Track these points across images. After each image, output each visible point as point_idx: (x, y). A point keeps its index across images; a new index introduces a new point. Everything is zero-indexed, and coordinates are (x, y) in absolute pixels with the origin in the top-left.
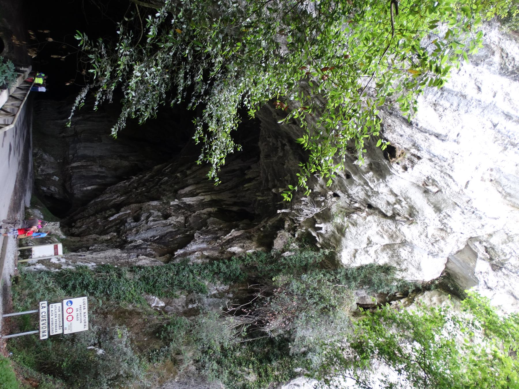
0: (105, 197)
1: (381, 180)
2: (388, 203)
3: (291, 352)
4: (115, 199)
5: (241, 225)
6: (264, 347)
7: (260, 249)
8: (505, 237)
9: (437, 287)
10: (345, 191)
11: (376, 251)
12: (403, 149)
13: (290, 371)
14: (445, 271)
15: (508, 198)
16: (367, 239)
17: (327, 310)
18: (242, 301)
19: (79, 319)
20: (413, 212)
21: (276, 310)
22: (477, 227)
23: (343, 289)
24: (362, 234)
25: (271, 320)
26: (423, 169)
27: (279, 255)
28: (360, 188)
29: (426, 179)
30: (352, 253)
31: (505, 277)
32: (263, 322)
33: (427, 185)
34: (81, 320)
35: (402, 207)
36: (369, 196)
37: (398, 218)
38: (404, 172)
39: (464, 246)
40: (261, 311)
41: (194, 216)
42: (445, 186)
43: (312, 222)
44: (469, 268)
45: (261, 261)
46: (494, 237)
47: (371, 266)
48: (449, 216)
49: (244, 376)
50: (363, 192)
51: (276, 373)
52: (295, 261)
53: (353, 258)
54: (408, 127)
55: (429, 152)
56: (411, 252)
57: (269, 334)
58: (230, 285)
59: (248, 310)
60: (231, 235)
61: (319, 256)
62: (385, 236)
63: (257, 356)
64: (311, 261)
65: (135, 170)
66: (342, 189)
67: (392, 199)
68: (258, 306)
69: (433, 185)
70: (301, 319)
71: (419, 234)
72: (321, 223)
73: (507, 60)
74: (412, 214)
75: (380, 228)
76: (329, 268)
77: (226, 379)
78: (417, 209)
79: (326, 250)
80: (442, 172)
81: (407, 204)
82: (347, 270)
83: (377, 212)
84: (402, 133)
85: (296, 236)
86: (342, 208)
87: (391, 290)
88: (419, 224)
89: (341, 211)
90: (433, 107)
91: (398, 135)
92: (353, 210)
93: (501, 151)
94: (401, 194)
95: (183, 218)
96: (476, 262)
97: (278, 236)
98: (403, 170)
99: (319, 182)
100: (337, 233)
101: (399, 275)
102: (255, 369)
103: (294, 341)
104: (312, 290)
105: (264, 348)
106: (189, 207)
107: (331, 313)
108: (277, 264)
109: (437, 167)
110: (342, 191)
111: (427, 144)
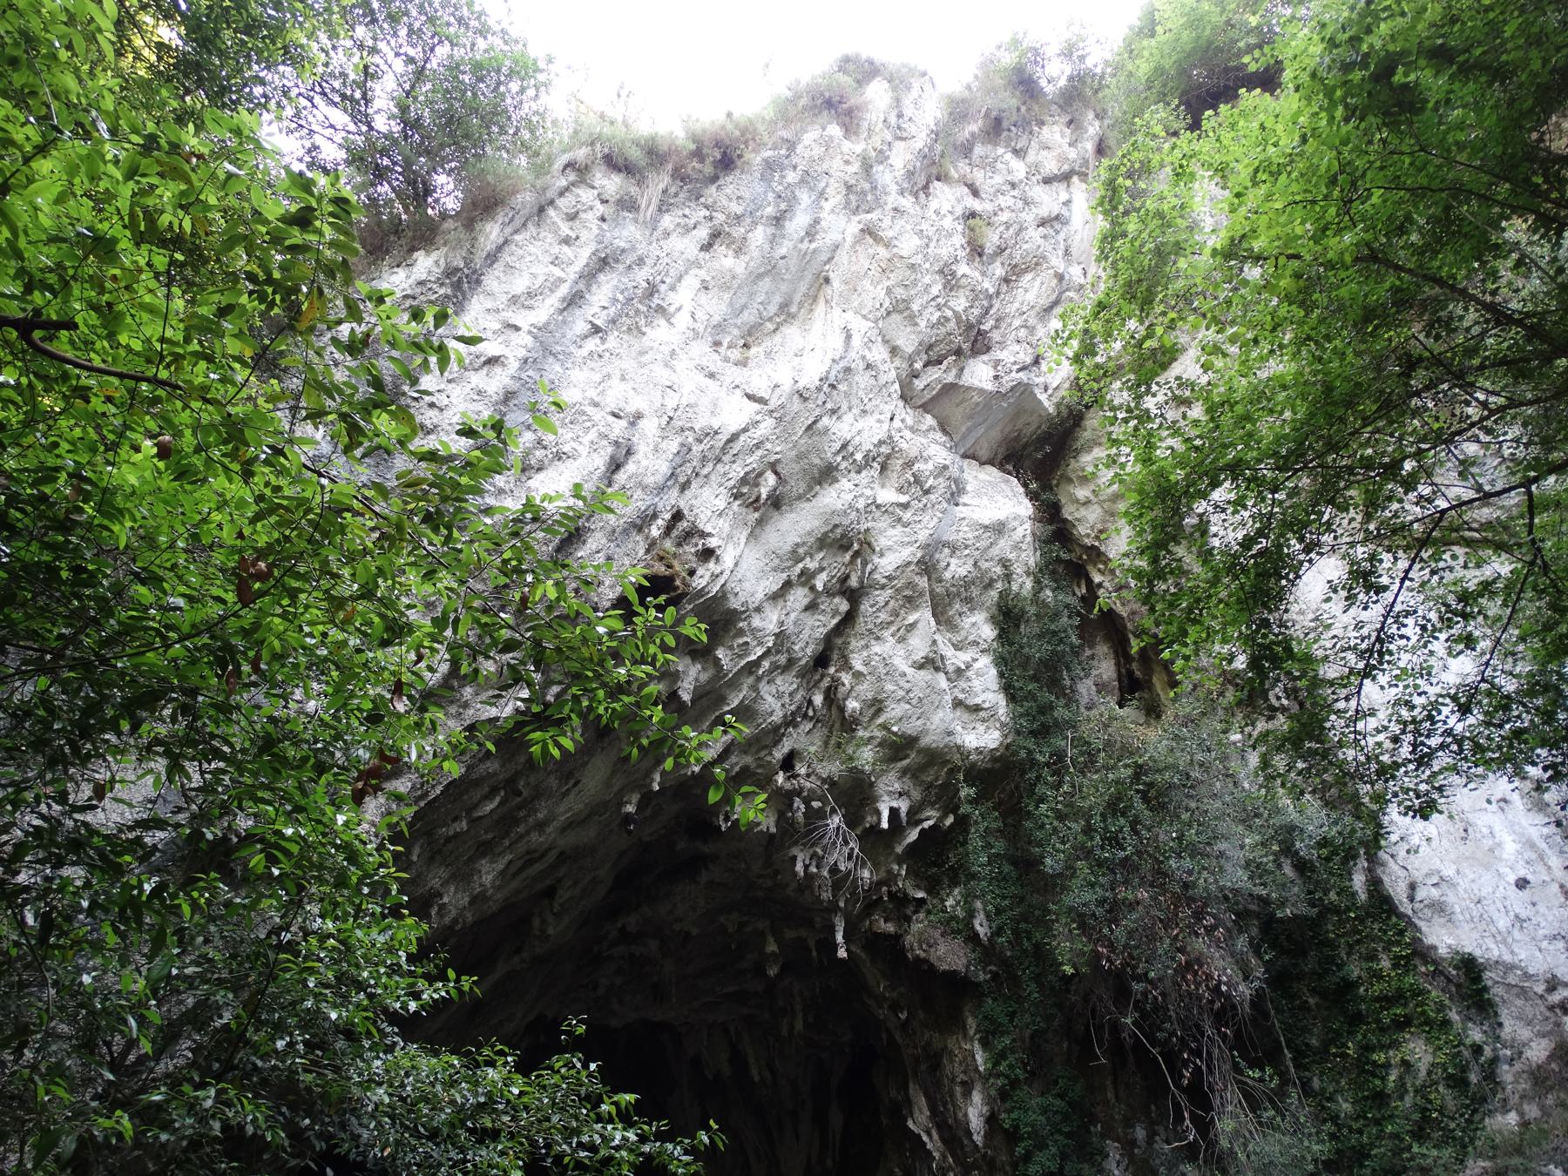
2: (811, 607)
3: (1304, 909)
5: (893, 1093)
6: (1304, 1007)
7: (971, 1023)
8: (896, 317)
9: (1046, 486)
10: (775, 734)
11: (957, 647)
12: (648, 557)
13: (1368, 915)
14: (1001, 468)
15: (793, 309)
16: (922, 672)
17: (1152, 793)
18: (1157, 1091)
20: (836, 540)
21: (1173, 959)
22: (873, 381)
23: (1080, 742)
24: (907, 686)
25: (1209, 977)
26: (709, 504)
27: (986, 951)
28: (764, 688)
30: (966, 716)
31: (1003, 325)
32: (1217, 1005)
33: (757, 499)
35: (822, 569)
36: (791, 662)
37: (854, 582)
38: (717, 559)
39: (929, 417)
40: (1183, 1013)
42: (759, 453)
43: (875, 841)
44: (987, 406)
45: (1012, 1015)
46: (899, 343)
47: (1001, 662)
48: (844, 446)
49: (1418, 1083)
50: (779, 681)
51: (1385, 963)
52: (1004, 898)
53: (983, 714)
54: (584, 542)
56: (954, 549)
57: (1256, 984)
58: (1103, 1136)
59: (1185, 1063)
60: (929, 1134)
61: (983, 820)
62: (911, 619)
63: (1338, 1034)
64: (999, 846)
66: (768, 742)
67: (799, 597)
68: (1167, 1025)
69: (757, 485)
70: (1190, 873)
71: (899, 528)
72: (878, 813)
73: (422, 298)
74: (845, 542)
75: (886, 634)
76: (1017, 787)
77: (1448, 1153)
79: (962, 794)
80: (719, 460)
82: (1018, 733)
83: (839, 641)
84: (600, 559)
85: (920, 895)
86: (826, 744)
87: (1067, 606)
89: (839, 745)
92: (834, 711)
93: (668, 321)
94: (783, 571)
96: (969, 388)
97: (923, 955)
98: (713, 561)
100: (905, 762)
101: (1024, 585)
102: (1386, 1040)
103: (1265, 901)
104: (1092, 839)
105: (1309, 1009)
107: (1158, 777)
108: (1016, 960)
109: (705, 471)
110: (777, 743)
111: (638, 494)
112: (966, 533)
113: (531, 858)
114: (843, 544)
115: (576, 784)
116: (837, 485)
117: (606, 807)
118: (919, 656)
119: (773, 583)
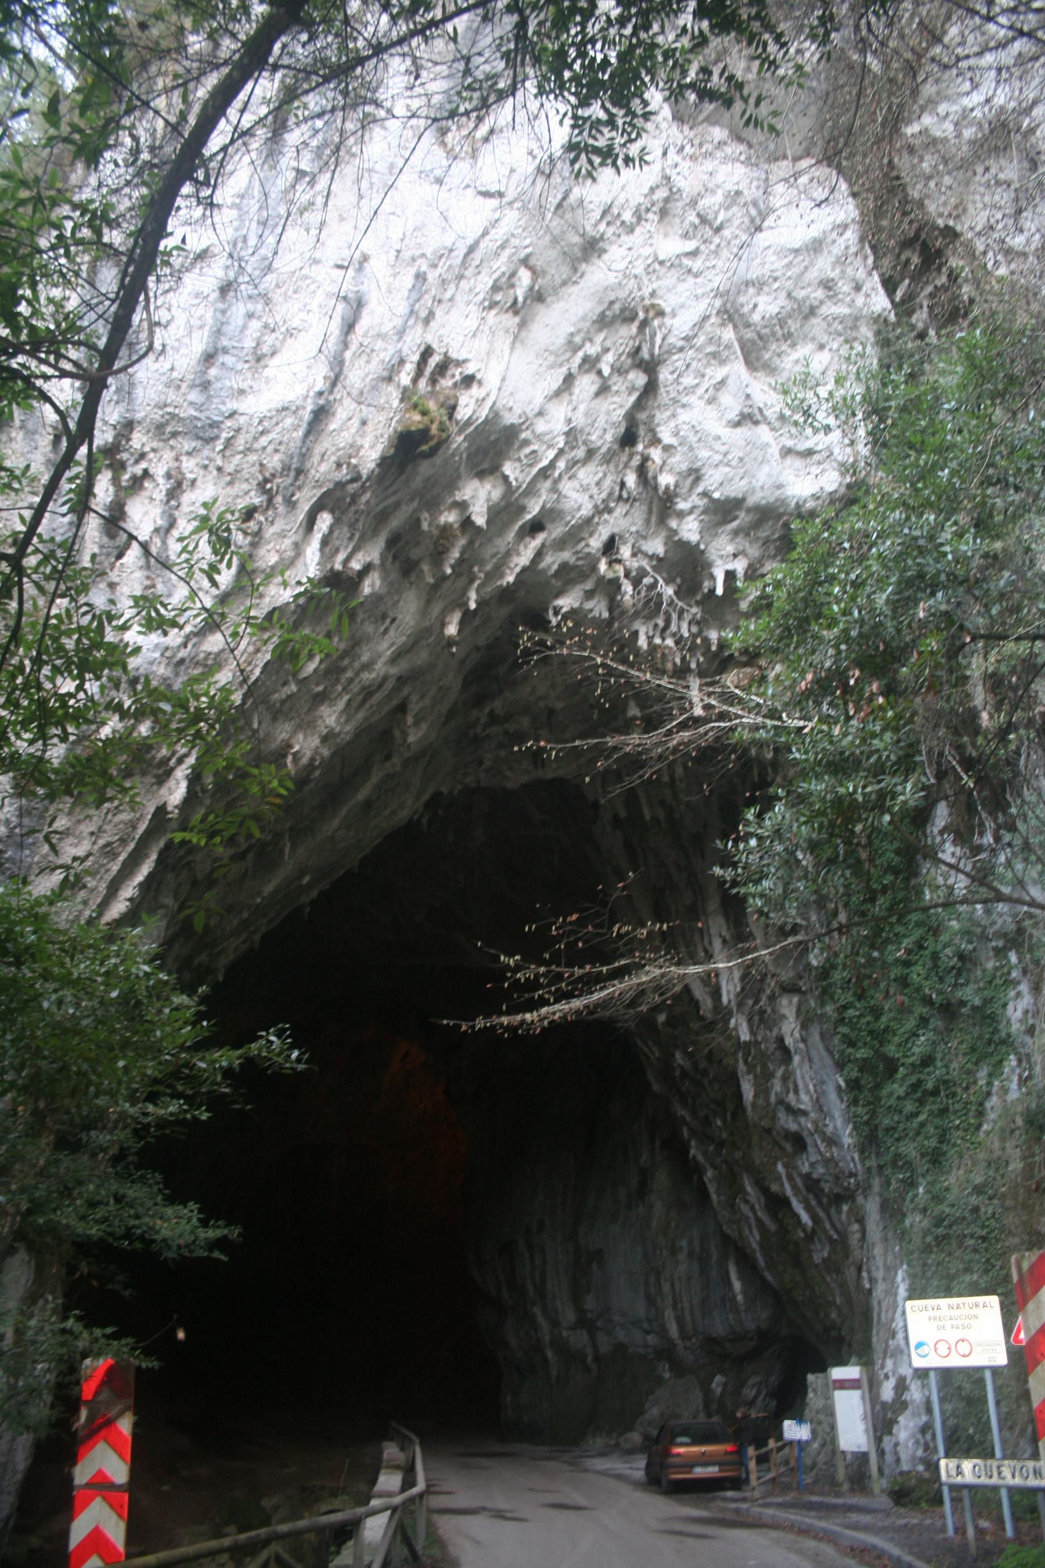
0: (754, 1239)
1: (523, 436)
2: (603, 390)
4: (752, 1208)
16: (739, 430)
19: (966, 1322)
24: (724, 449)
26: (462, 330)
28: (567, 487)
29: (493, 312)
30: (798, 462)
34: (969, 1317)
36: (591, 453)
38: (480, 383)
42: (507, 252)
53: (816, 457)
55: (401, 333)
56: (759, 285)
65: (676, 1150)
67: (586, 384)
69: (513, 286)
71: (691, 280)
72: (713, 578)
78: (600, 309)
80: (461, 277)
81: (591, 341)
83: (642, 416)
84: (355, 423)
88: (655, 285)
90: (266, 360)
91: (363, 437)
94: (561, 365)
95: (784, 1001)
99: (576, 605)
100: (735, 524)
109: (448, 295)
112: (774, 263)
113: (368, 692)
114: (627, 316)
115: (393, 620)
116: (605, 257)
117: (427, 634)
118: (733, 415)
119: (555, 379)
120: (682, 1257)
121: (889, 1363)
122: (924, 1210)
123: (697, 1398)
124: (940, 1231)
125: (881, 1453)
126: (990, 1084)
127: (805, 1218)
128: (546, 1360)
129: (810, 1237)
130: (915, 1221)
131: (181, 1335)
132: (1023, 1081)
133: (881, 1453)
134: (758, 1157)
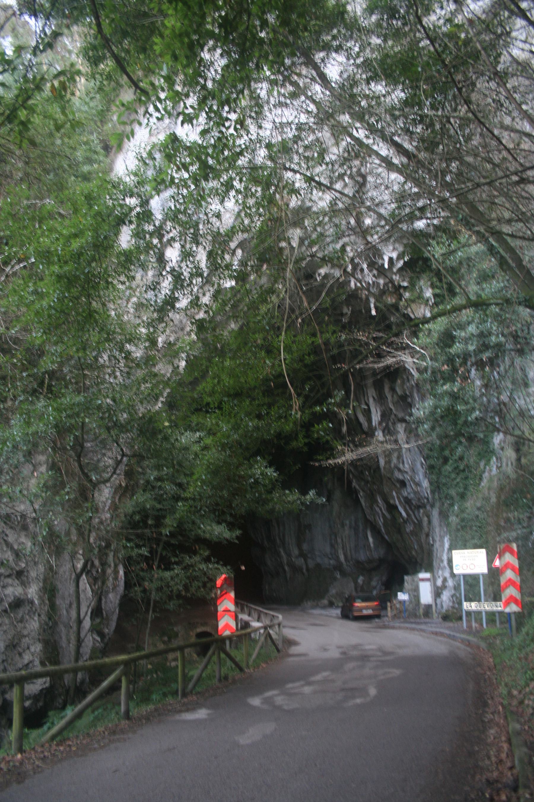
0: (380, 522)
4: (381, 509)
41: (397, 410)
72: (383, 259)
106: (385, 416)
120: (346, 528)
121: (440, 572)
122: (457, 516)
123: (352, 585)
124: (463, 524)
125: (436, 604)
126: (485, 468)
127: (404, 514)
128: (285, 571)
129: (405, 522)
130: (453, 519)
131: (243, 568)
132: (498, 468)
133: (436, 604)
134: (386, 489)
